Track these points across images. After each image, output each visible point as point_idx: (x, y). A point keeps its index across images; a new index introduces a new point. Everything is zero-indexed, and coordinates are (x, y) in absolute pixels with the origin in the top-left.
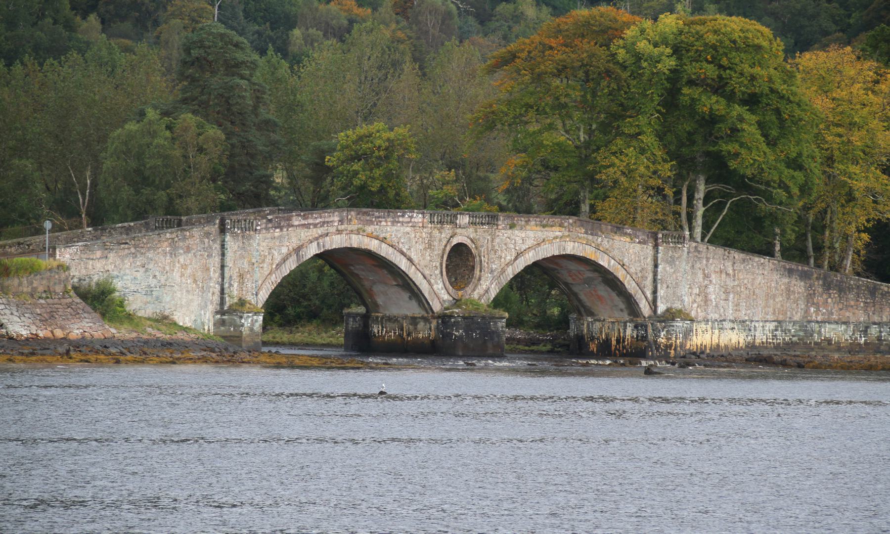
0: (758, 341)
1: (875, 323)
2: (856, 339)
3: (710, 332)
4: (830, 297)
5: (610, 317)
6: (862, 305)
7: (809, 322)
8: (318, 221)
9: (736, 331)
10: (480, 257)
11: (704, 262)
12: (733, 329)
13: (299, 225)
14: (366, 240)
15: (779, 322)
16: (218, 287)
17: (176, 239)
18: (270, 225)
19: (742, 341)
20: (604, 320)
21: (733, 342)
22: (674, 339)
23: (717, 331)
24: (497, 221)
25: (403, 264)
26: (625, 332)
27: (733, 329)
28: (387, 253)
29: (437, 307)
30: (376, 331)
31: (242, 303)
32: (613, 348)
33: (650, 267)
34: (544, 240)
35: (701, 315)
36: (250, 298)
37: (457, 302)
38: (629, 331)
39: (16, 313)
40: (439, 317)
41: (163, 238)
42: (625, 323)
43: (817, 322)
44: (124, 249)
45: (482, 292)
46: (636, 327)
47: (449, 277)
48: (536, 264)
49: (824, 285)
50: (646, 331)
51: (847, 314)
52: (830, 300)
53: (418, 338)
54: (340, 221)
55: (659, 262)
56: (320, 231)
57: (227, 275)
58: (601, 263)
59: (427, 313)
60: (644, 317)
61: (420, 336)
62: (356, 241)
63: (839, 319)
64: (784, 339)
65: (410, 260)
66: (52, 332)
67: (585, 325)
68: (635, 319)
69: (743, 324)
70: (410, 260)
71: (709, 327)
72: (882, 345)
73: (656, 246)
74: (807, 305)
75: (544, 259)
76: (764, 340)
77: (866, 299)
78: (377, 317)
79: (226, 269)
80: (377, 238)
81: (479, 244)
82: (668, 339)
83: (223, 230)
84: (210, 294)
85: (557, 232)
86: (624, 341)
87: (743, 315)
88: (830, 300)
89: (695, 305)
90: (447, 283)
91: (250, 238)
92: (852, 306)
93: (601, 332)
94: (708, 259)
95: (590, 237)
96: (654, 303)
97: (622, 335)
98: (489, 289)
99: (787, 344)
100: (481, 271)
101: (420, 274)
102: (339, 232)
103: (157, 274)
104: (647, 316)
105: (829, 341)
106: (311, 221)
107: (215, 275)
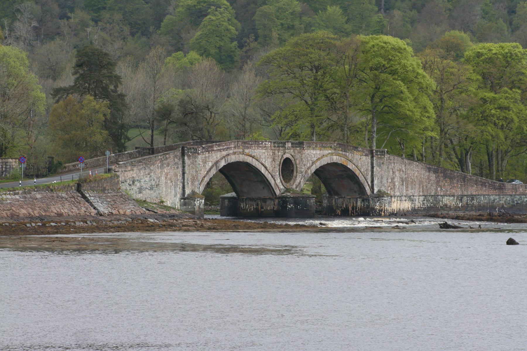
0: (416, 207)
1: (465, 196)
2: (458, 204)
3: (396, 202)
4: (446, 182)
5: (348, 196)
6: (460, 186)
7: (438, 196)
8: (225, 147)
9: (407, 201)
10: (296, 165)
11: (393, 165)
12: (406, 200)
13: (216, 150)
14: (246, 157)
15: (425, 196)
16: (181, 184)
17: (163, 159)
18: (204, 150)
19: (410, 207)
20: (345, 197)
21: (406, 207)
22: (383, 206)
23: (399, 202)
24: (303, 145)
25: (263, 170)
26: (357, 203)
27: (406, 200)
28: (255, 164)
29: (278, 192)
30: (242, 206)
31: (193, 193)
32: (350, 212)
33: (370, 168)
34: (324, 155)
35: (392, 193)
36: (197, 190)
37: (287, 190)
38: (359, 203)
39: (99, 201)
40: (279, 198)
41: (157, 159)
42: (357, 199)
43: (441, 196)
44: (140, 165)
45: (297, 184)
46: (363, 201)
47: (283, 177)
48: (321, 167)
49: (444, 176)
50: (369, 203)
51: (454, 191)
52: (446, 184)
53: (267, 210)
54: (234, 147)
55: (374, 165)
56: (224, 153)
57: (186, 178)
58: (349, 167)
59: (273, 196)
60: (368, 195)
61: (269, 208)
62: (241, 158)
63: (450, 194)
64: (427, 205)
65: (266, 167)
66: (119, 212)
67: (334, 201)
68: (363, 196)
69: (410, 198)
70: (266, 167)
71: (396, 199)
72: (468, 207)
73: (372, 157)
74: (436, 187)
75: (324, 165)
76: (419, 206)
77: (461, 182)
78: (243, 199)
79: (186, 175)
80: (251, 156)
81: (296, 158)
82: (381, 207)
83: (183, 154)
84: (178, 189)
85: (326, 152)
86: (356, 208)
87: (410, 193)
88: (446, 184)
89: (390, 188)
90: (282, 179)
91: (196, 157)
92: (455, 187)
93: (343, 204)
94: (394, 163)
95: (344, 153)
96: (372, 188)
97: (355, 205)
98: (300, 182)
99: (428, 207)
100: (297, 173)
101: (270, 175)
102: (234, 153)
103: (155, 178)
104: (369, 194)
105: (446, 205)
106: (221, 148)
107: (180, 178)
